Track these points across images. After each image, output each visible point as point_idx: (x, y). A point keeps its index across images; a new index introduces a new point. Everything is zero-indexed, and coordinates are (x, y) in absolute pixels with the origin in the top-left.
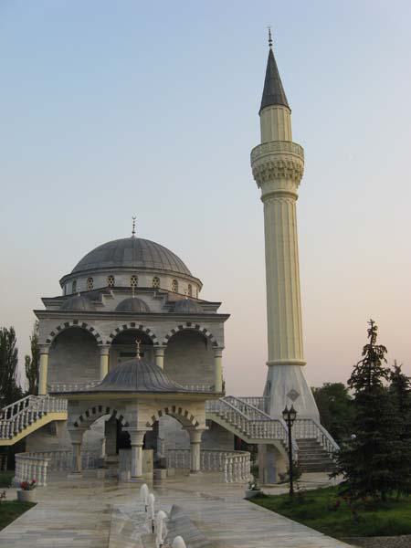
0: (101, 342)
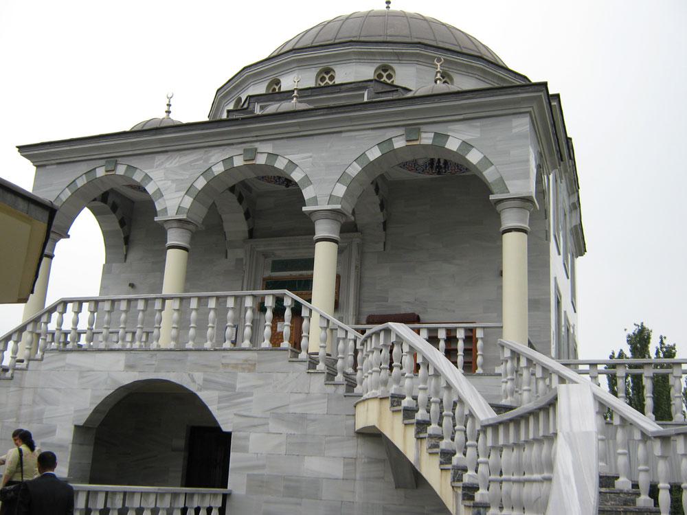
0: (165, 210)
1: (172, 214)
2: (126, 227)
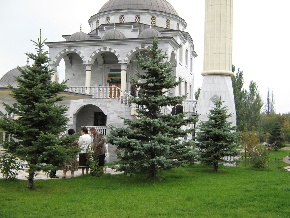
1: (87, 62)
2: (71, 59)
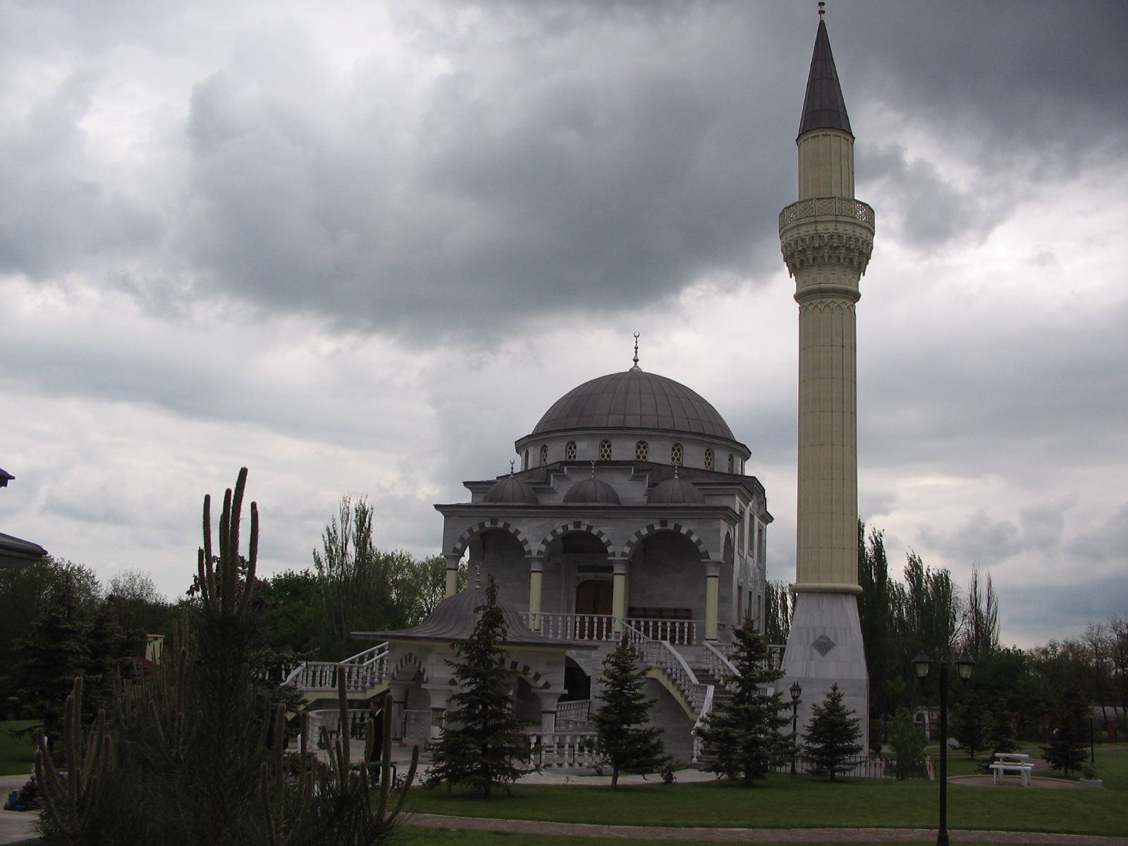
0: (530, 552)
